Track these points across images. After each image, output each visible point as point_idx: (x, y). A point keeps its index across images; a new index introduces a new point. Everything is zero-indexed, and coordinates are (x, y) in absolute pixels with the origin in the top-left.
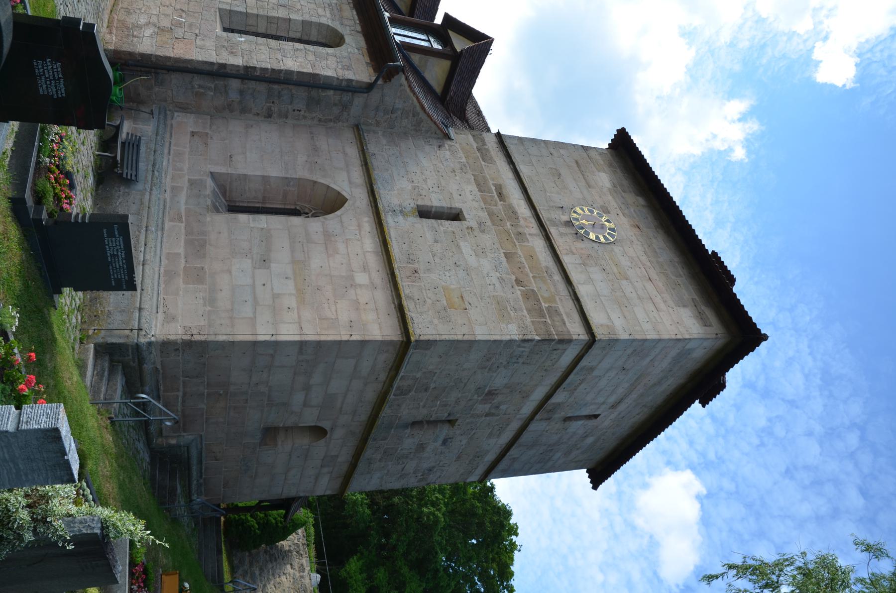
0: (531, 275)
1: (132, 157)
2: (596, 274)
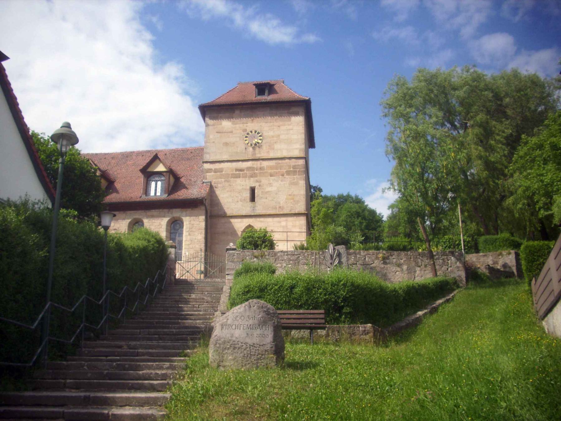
0: (279, 170)
1: (310, 314)
2: (277, 146)
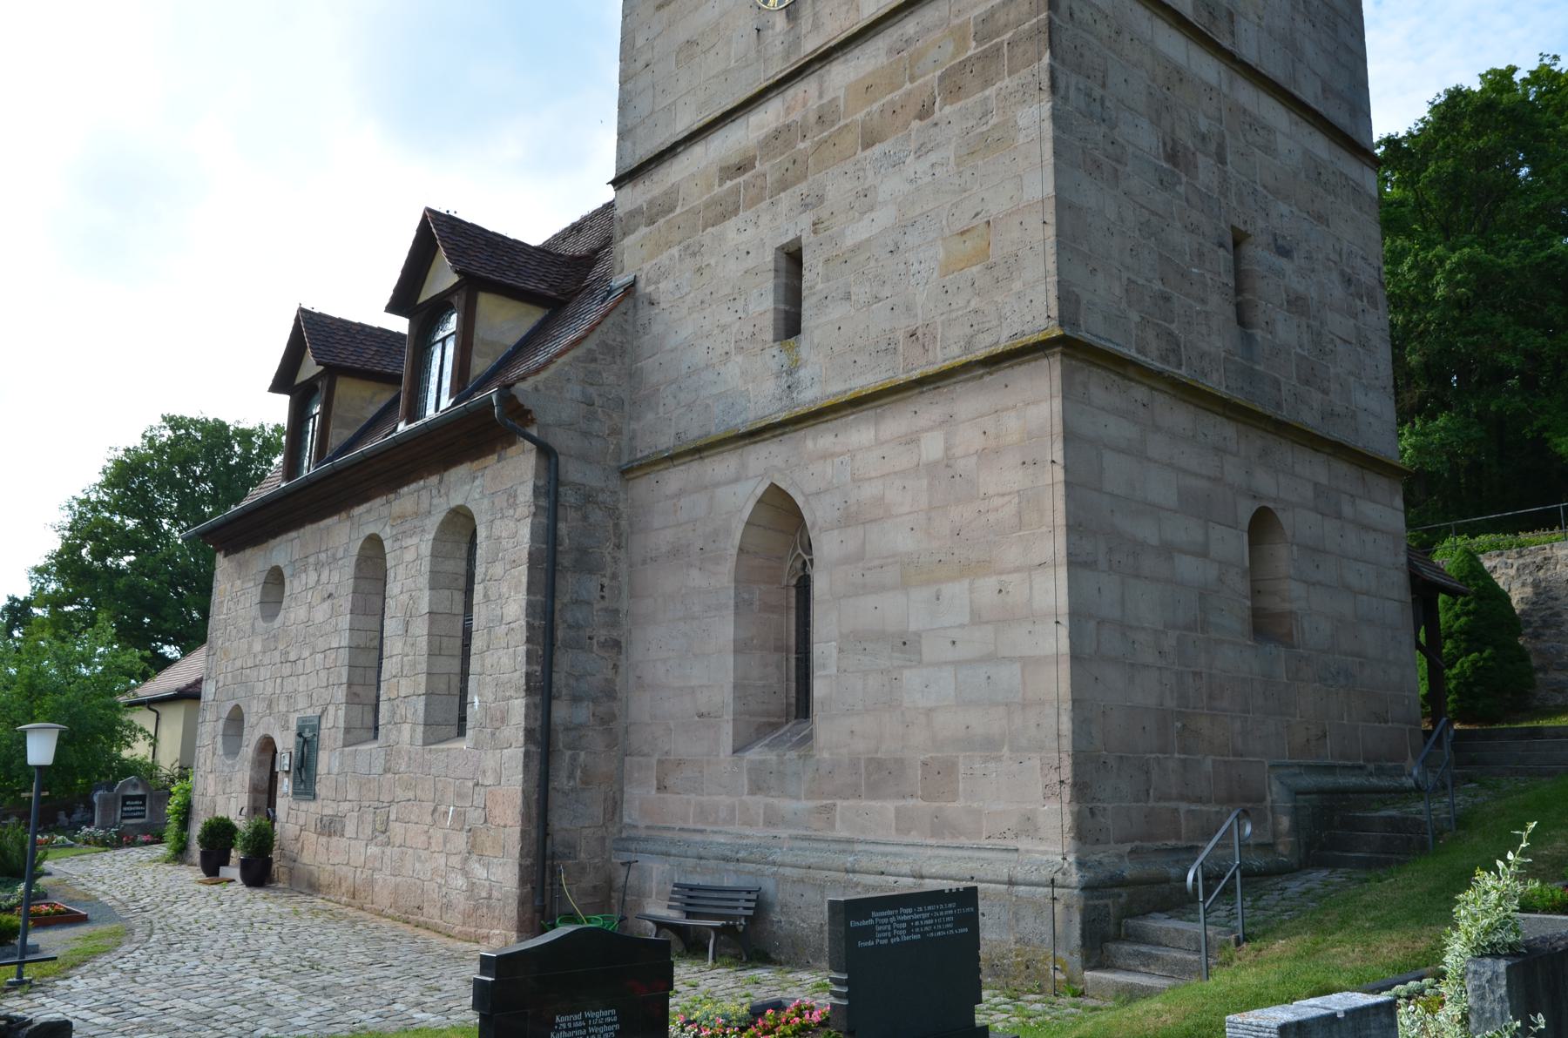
0: (908, 86)
